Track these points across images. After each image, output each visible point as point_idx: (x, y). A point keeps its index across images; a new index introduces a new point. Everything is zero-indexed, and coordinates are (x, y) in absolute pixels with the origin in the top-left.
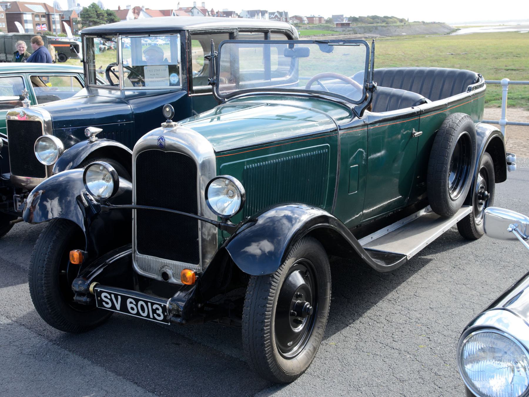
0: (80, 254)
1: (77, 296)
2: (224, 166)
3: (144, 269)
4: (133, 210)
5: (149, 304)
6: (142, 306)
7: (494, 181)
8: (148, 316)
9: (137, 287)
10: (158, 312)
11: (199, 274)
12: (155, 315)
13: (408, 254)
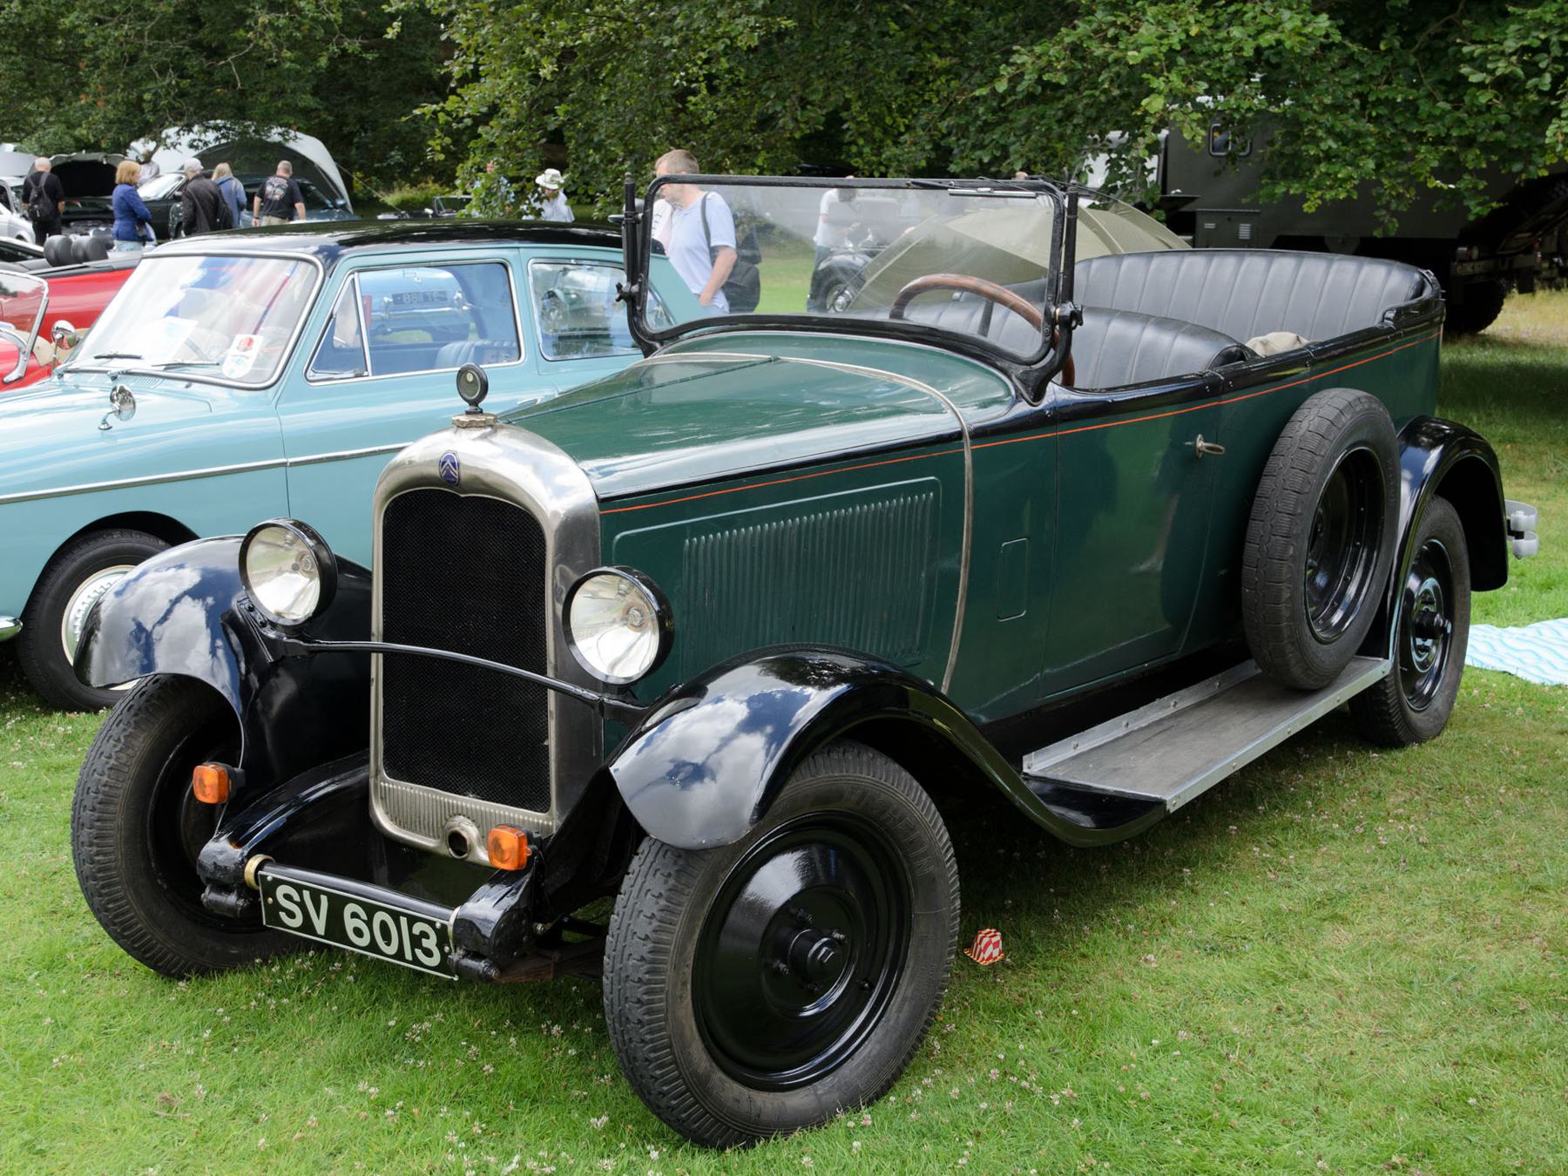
0: (220, 776)
1: (211, 890)
2: (624, 537)
3: (401, 824)
4: (374, 656)
5: (403, 920)
6: (384, 925)
7: (1468, 583)
8: (400, 955)
9: (383, 872)
10: (425, 943)
11: (540, 843)
12: (418, 952)
13: (1167, 798)
